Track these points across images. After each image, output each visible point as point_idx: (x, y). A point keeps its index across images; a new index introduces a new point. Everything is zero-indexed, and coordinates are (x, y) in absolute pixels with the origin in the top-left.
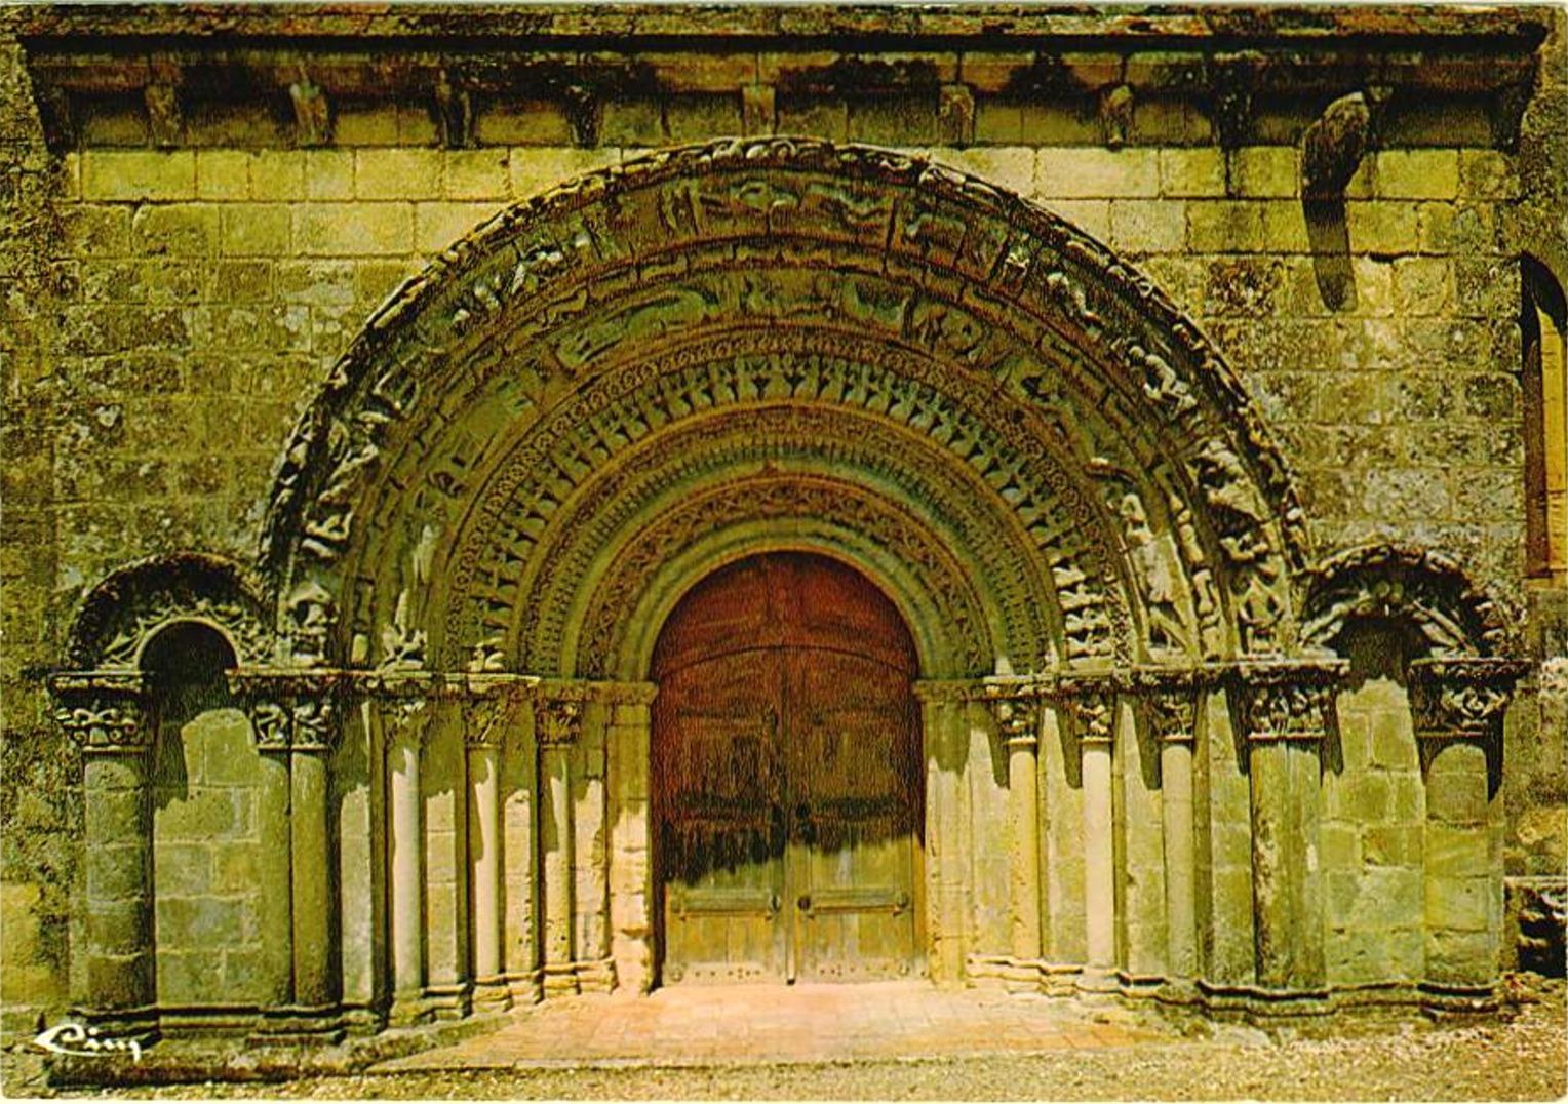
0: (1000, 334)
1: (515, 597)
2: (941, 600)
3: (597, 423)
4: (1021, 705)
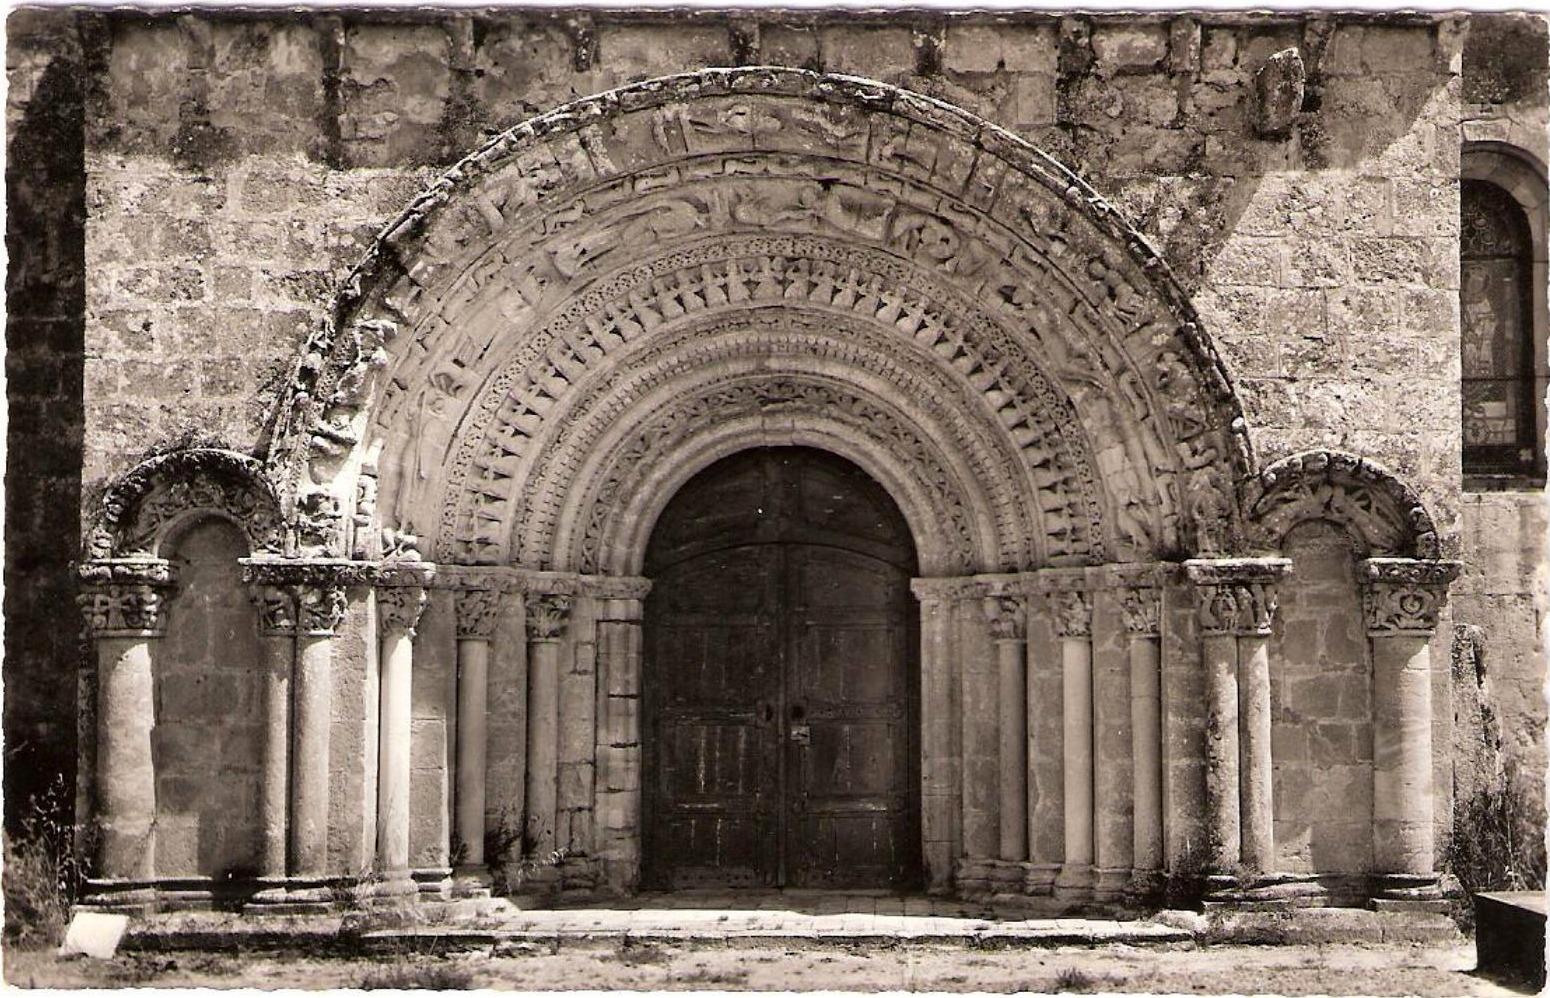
0: (976, 245)
1: (509, 489)
2: (937, 495)
3: (592, 325)
4: (1008, 604)
